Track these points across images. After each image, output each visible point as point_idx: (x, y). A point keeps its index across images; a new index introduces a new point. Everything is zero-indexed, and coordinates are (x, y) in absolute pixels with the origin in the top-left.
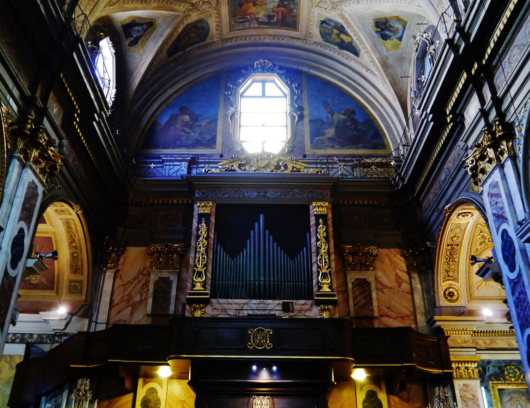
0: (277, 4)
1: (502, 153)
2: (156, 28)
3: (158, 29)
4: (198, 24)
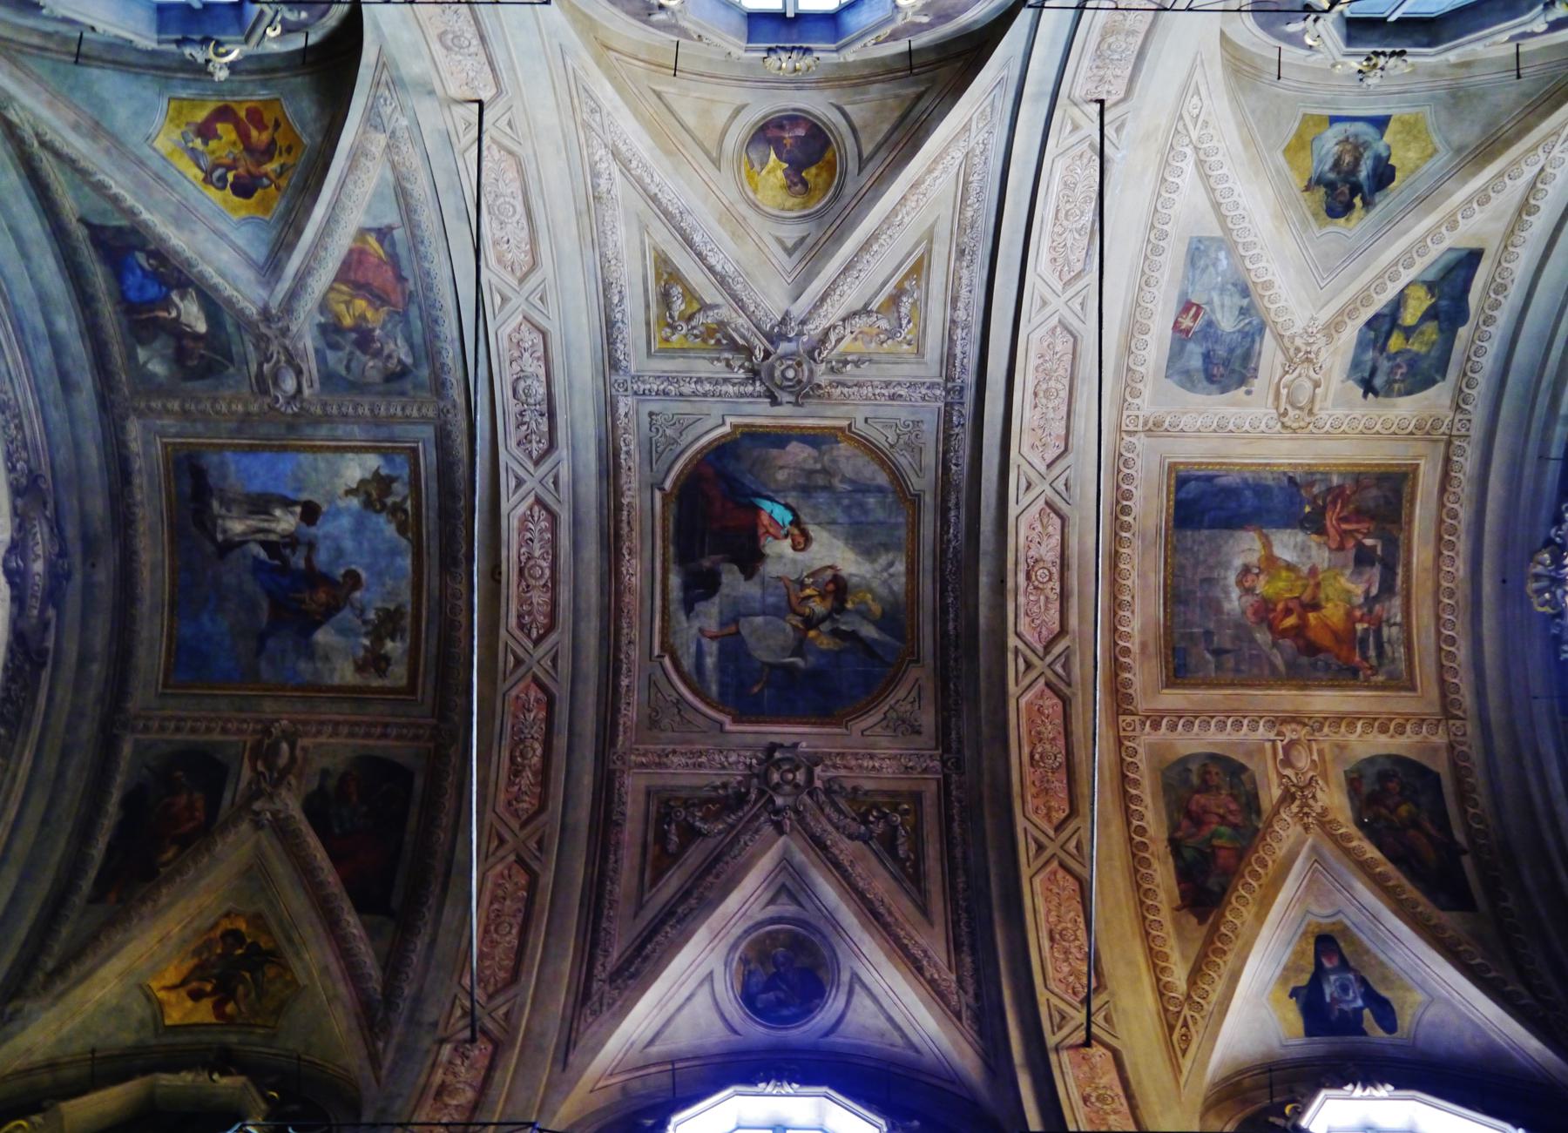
0: (1314, 537)
2: (1345, 929)
3: (1349, 923)
4: (1366, 789)
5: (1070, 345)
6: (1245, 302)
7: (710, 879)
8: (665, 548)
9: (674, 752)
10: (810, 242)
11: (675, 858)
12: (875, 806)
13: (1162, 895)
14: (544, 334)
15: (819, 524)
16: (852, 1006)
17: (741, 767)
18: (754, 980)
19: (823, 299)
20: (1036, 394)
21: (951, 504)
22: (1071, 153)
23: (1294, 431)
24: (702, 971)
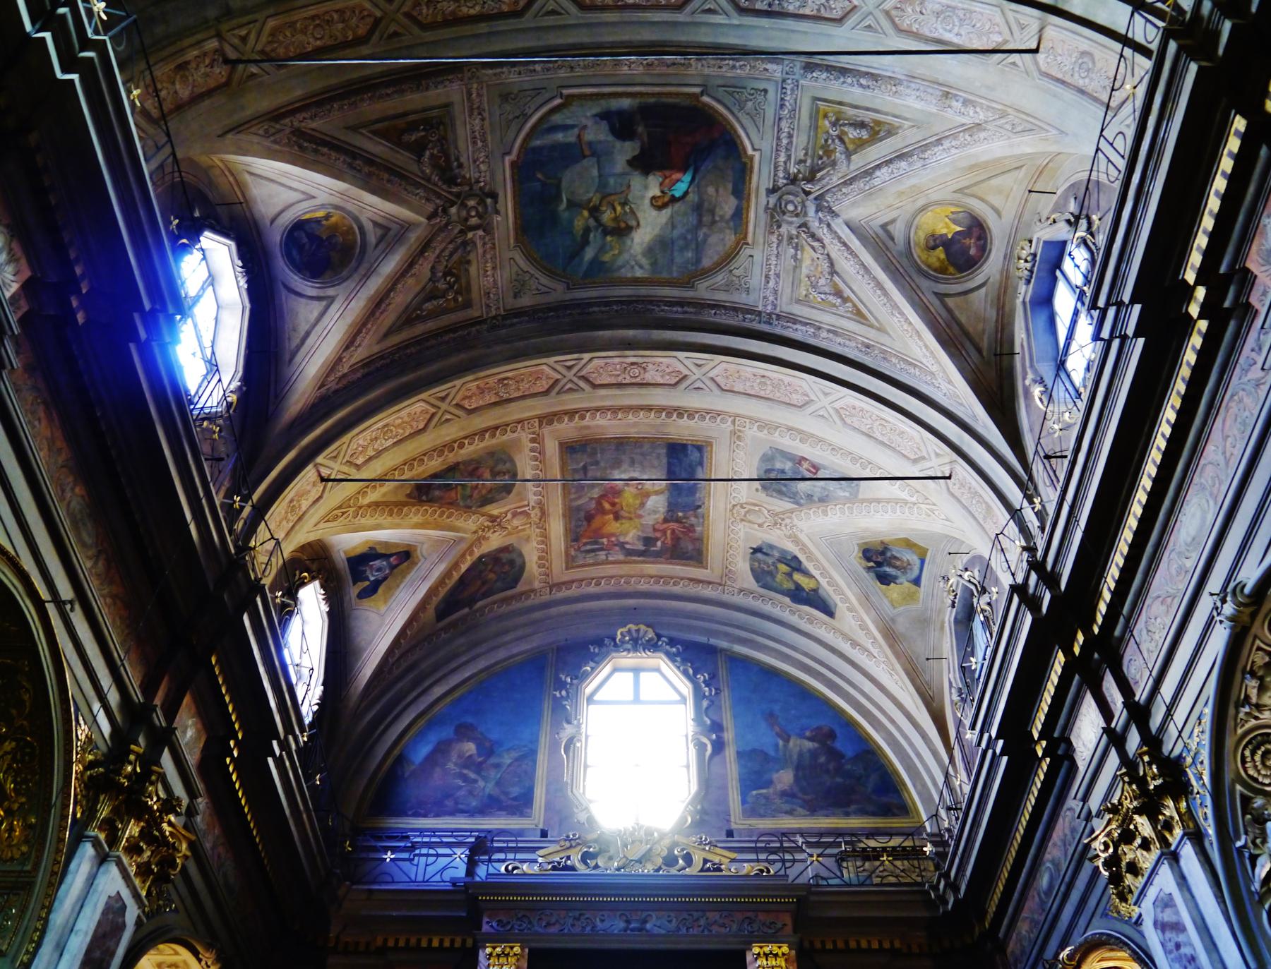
1: (1168, 826)
4: (505, 557)
5: (796, 403)
6: (816, 499)
7: (386, 176)
8: (653, 95)
9: (483, 119)
10: (890, 244)
11: (399, 144)
12: (458, 278)
13: (421, 469)
14: (839, 21)
15: (672, 217)
16: (310, 302)
17: (477, 175)
18: (314, 225)
19: (845, 244)
20: (763, 376)
21: (686, 309)
22: (922, 444)
23: (731, 511)
24: (313, 192)
